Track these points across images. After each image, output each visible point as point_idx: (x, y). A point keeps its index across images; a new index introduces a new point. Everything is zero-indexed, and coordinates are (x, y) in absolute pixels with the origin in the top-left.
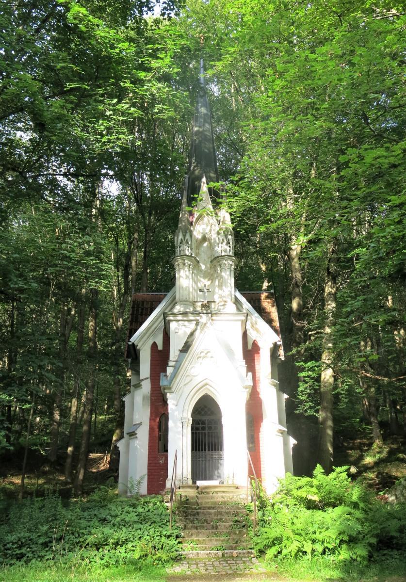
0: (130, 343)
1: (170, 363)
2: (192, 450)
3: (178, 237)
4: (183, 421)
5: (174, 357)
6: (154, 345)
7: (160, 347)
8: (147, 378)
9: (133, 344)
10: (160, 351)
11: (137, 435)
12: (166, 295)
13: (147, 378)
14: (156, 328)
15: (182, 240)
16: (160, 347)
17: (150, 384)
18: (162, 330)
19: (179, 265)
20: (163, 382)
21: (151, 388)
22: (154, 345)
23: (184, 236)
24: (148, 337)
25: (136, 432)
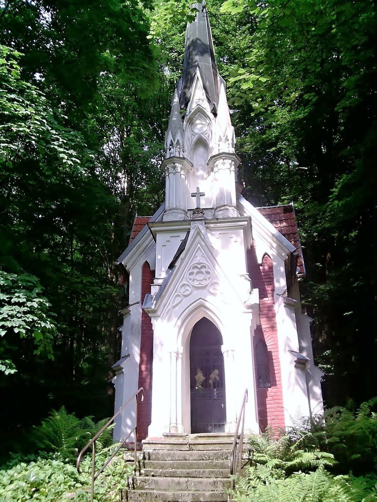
14: (147, 246)
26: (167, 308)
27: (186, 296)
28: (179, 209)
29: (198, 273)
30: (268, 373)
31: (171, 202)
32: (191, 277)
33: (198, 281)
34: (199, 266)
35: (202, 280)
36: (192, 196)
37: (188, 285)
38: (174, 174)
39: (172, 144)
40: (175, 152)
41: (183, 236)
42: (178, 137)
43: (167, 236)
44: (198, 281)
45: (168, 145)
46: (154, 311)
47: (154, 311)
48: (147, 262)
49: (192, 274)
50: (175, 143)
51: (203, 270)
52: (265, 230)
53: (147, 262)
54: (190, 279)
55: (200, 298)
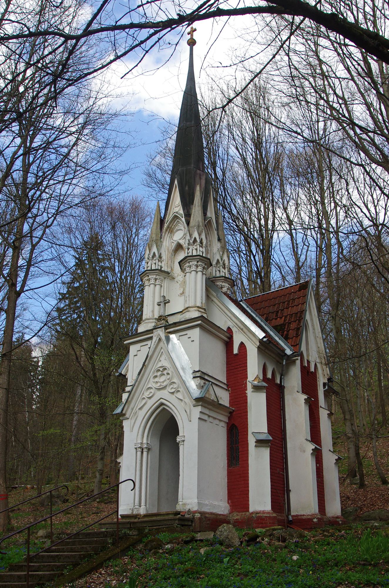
49: (156, 377)
55: (161, 398)
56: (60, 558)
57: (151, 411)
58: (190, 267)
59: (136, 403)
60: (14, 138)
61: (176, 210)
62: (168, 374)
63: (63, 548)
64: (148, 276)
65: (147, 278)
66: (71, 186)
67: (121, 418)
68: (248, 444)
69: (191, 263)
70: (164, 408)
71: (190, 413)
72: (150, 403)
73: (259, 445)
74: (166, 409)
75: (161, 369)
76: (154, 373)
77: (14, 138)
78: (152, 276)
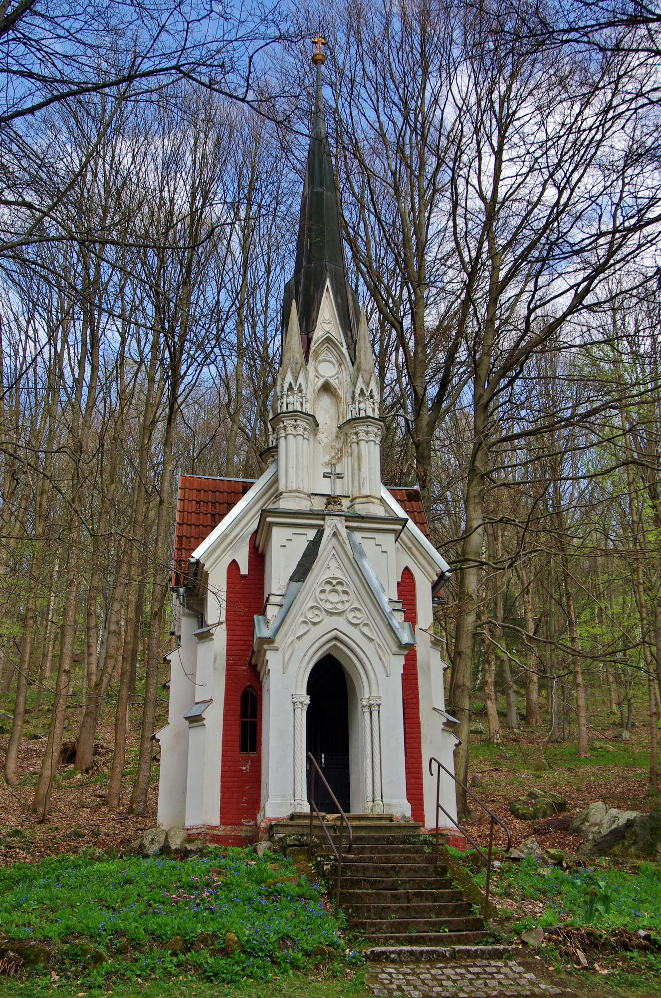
0: (193, 560)
1: (273, 599)
2: (309, 749)
3: (284, 379)
4: (294, 700)
5: (279, 589)
6: (234, 565)
7: (244, 570)
8: (220, 623)
9: (198, 561)
10: (244, 576)
11: (205, 722)
12: (253, 483)
13: (220, 623)
14: (236, 536)
15: (290, 384)
16: (244, 570)
17: (225, 633)
18: (248, 540)
19: (285, 428)
20: (262, 631)
21: (228, 640)
22: (234, 565)
23: (296, 379)
24: (224, 551)
25: (204, 716)
26: (366, 673)
27: (315, 624)
28: (300, 492)
29: (332, 591)
30: (140, 591)
31: (290, 480)
32: (323, 596)
33: (332, 603)
34: (334, 582)
35: (336, 603)
36: (325, 477)
37: (318, 608)
38: (367, 442)
39: (291, 388)
40: (293, 402)
41: (311, 534)
42: (301, 380)
43: (288, 532)
44: (332, 603)
45: (285, 390)
46: (270, 640)
47: (270, 640)
48: (234, 561)
49: (323, 591)
50: (296, 389)
51: (339, 588)
52: (412, 538)
53: (234, 561)
54: (322, 600)
55: (336, 629)
56: (399, 871)
57: (317, 645)
58: (367, 433)
59: (294, 627)
60: (180, 12)
61: (327, 327)
62: (345, 592)
63: (372, 858)
64: (296, 420)
65: (365, 428)
66: (611, 227)
67: (265, 647)
68: (419, 723)
69: (370, 429)
70: (335, 645)
71: (289, 659)
72: (316, 632)
73: (446, 728)
74: (338, 648)
75: (334, 582)
76: (321, 585)
77: (180, 12)
78: (289, 422)
